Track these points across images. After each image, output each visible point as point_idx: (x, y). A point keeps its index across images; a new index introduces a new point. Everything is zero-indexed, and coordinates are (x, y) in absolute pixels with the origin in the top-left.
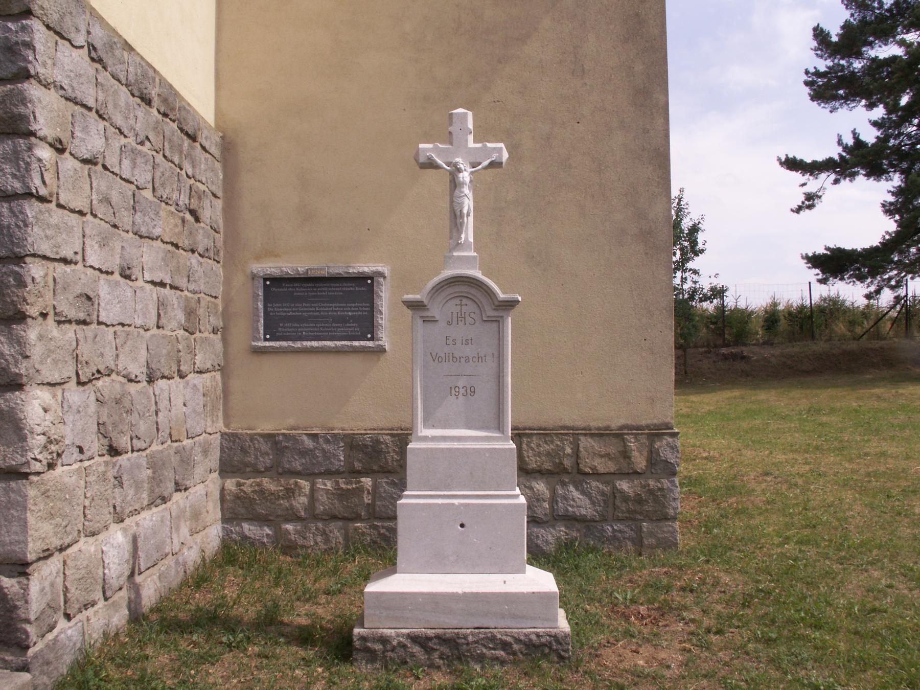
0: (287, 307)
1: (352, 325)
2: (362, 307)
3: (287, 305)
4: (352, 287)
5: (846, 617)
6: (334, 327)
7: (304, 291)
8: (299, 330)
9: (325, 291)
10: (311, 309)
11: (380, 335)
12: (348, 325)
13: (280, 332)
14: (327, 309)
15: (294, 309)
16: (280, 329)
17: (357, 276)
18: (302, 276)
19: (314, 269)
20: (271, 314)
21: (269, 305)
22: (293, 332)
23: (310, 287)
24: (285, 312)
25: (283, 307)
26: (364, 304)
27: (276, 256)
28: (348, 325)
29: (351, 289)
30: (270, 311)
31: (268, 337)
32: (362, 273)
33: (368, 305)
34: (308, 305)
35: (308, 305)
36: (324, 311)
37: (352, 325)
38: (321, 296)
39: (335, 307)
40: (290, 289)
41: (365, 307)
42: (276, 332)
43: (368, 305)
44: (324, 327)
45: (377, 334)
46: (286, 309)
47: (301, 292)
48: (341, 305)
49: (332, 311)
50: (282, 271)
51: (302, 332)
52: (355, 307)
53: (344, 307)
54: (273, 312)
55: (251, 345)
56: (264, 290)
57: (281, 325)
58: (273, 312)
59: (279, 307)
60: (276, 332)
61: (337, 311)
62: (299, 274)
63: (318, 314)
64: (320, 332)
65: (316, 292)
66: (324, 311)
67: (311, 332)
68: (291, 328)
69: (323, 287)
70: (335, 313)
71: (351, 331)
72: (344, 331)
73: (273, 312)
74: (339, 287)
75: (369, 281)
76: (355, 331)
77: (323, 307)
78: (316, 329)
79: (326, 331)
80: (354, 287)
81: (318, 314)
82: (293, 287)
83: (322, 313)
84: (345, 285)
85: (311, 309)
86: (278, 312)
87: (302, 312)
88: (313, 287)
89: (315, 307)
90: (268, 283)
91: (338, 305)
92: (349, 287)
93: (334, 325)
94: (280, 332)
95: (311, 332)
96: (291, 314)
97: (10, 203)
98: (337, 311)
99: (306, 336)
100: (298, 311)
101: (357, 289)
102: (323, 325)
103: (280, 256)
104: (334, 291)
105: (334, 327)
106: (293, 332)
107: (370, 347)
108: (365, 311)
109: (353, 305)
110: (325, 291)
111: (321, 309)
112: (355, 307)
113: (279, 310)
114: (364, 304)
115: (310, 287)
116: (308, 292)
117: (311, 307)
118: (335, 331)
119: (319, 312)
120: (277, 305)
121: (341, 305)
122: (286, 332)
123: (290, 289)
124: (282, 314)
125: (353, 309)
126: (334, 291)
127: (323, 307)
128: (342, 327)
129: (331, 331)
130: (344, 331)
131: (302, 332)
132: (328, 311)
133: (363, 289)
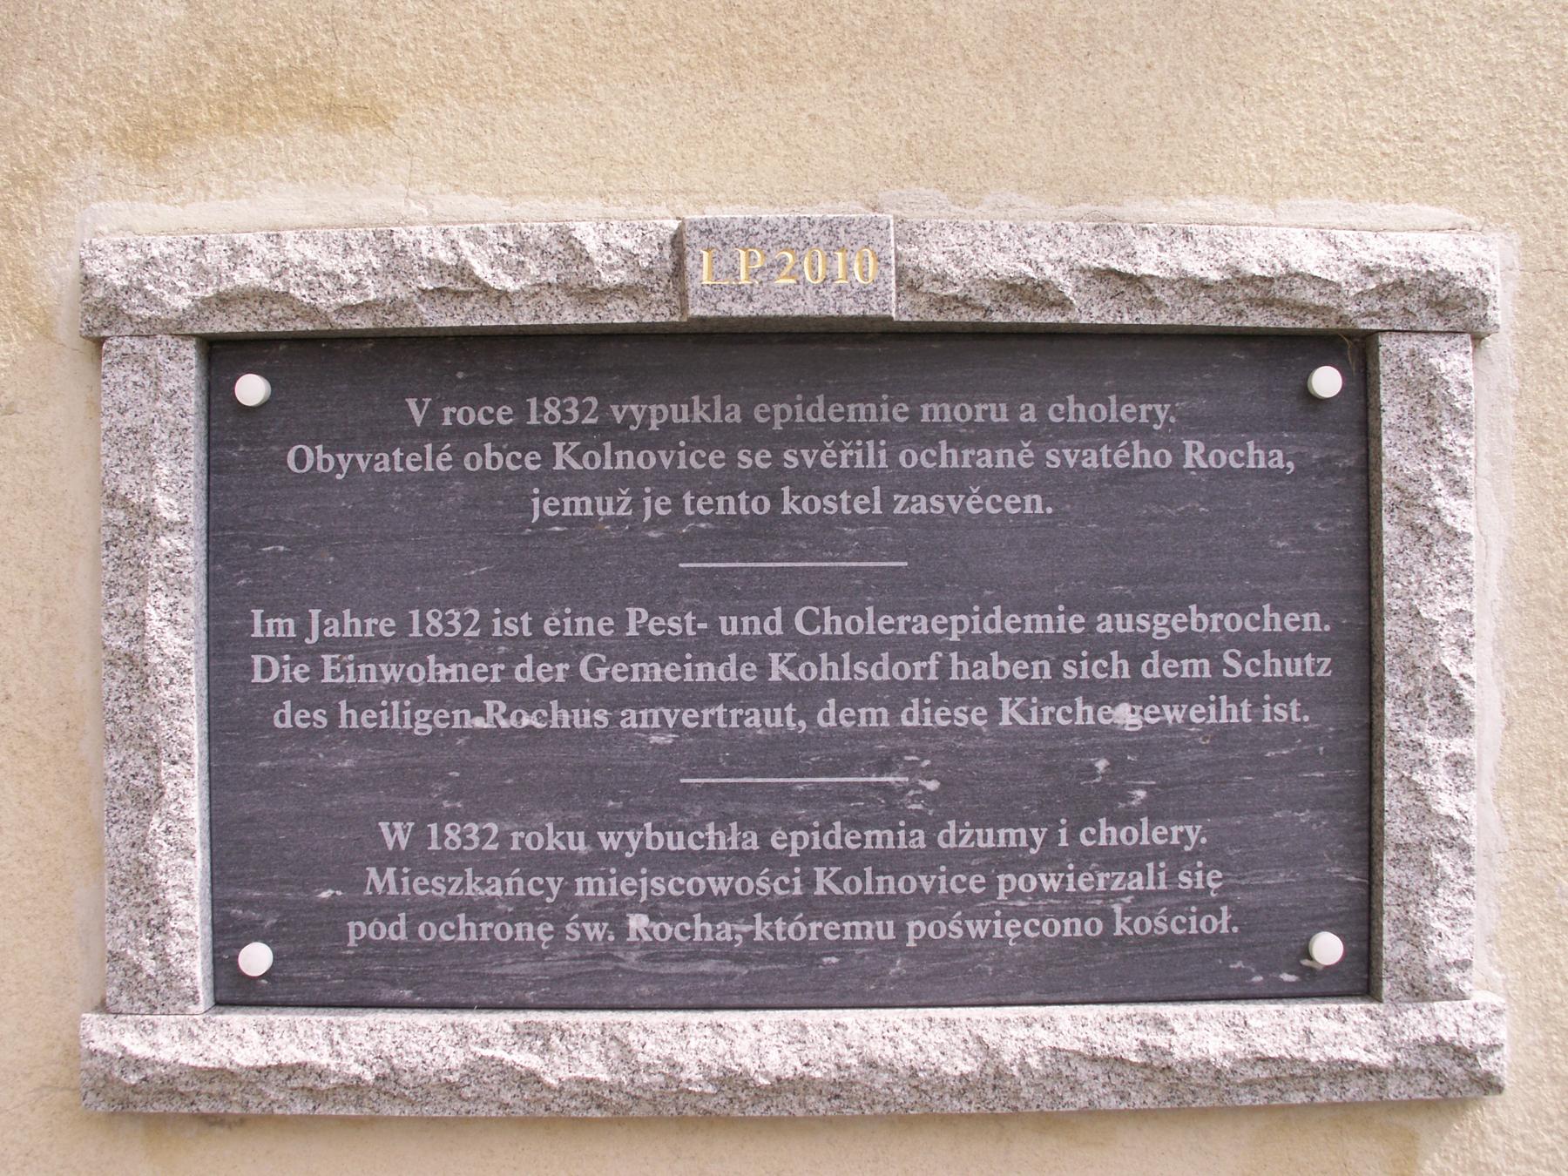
0: (451, 650)
1: (1148, 834)
2: (1250, 646)
3: (455, 622)
4: (1142, 432)
5: (1439, 1037)
6: (959, 861)
7: (633, 481)
8: (588, 887)
9: (858, 481)
10: (706, 672)
11: (1447, 946)
12: (1108, 834)
13: (383, 909)
14: (885, 670)
15: (528, 672)
16: (381, 881)
17: (1214, 316)
18: (620, 314)
19: (748, 234)
20: (287, 717)
21: (262, 625)
22: (524, 910)
23: (699, 436)
24: (433, 696)
25: (413, 652)
26: (1272, 621)
27: (334, 114)
28: (1108, 834)
29: (1141, 457)
30: (277, 693)
31: (256, 958)
32: (1263, 289)
33: (1312, 622)
34: (681, 625)
35: (681, 625)
36: (848, 694)
37: (1148, 834)
38: (823, 535)
39: (974, 648)
40: (489, 458)
41: (1286, 646)
42: (339, 913)
43: (1312, 622)
44: (849, 863)
45: (1415, 933)
46: (447, 673)
47: (607, 483)
48: (1038, 624)
49: (944, 691)
50: (396, 259)
51: (614, 913)
52: (1179, 647)
53: (1061, 648)
54: (304, 696)
55: (75, 1050)
56: (214, 467)
57: (396, 835)
58: (304, 696)
59: (367, 650)
60: (339, 913)
61: (988, 694)
62: (591, 294)
63: (783, 719)
64: (811, 907)
65: (768, 484)
66: (848, 694)
67: (715, 908)
68: (489, 866)
69: (846, 433)
70: (976, 717)
71: (1142, 903)
72: (1076, 906)
73: (312, 695)
74: (1011, 435)
75: (1327, 381)
76: (1178, 901)
77: (835, 646)
78: (763, 885)
79: (865, 907)
80: (1171, 439)
81: (783, 719)
82: (519, 437)
83: (830, 716)
84: (1075, 410)
85: (706, 672)
86: (363, 698)
87: (617, 698)
88: (727, 438)
89: (756, 650)
90: (252, 389)
91: (1000, 623)
92: (1112, 433)
93: (952, 836)
94: (383, 909)
95: (715, 908)
96: (495, 717)
97: (730, 708)
98: (988, 694)
99: (654, 952)
100: (573, 694)
101: (1194, 454)
102: (841, 838)
103: (379, 117)
104: (955, 482)
105: (959, 861)
106: (524, 910)
107: (1340, 1071)
108: (1283, 690)
109: (1160, 625)
110: (858, 481)
111: (824, 670)
112: (1179, 647)
113: (365, 675)
114: (1272, 621)
115: (699, 436)
116: (669, 483)
117: (709, 647)
118: (968, 905)
119: (806, 697)
120: (350, 625)
121: (1038, 624)
122: (440, 910)
123: (489, 458)
124: (393, 717)
125: (1156, 668)
126: (955, 482)
127: (835, 646)
128: (1050, 859)
129: (926, 905)
130: (1076, 906)
131: (614, 913)
132: (898, 695)
133: (1255, 456)
